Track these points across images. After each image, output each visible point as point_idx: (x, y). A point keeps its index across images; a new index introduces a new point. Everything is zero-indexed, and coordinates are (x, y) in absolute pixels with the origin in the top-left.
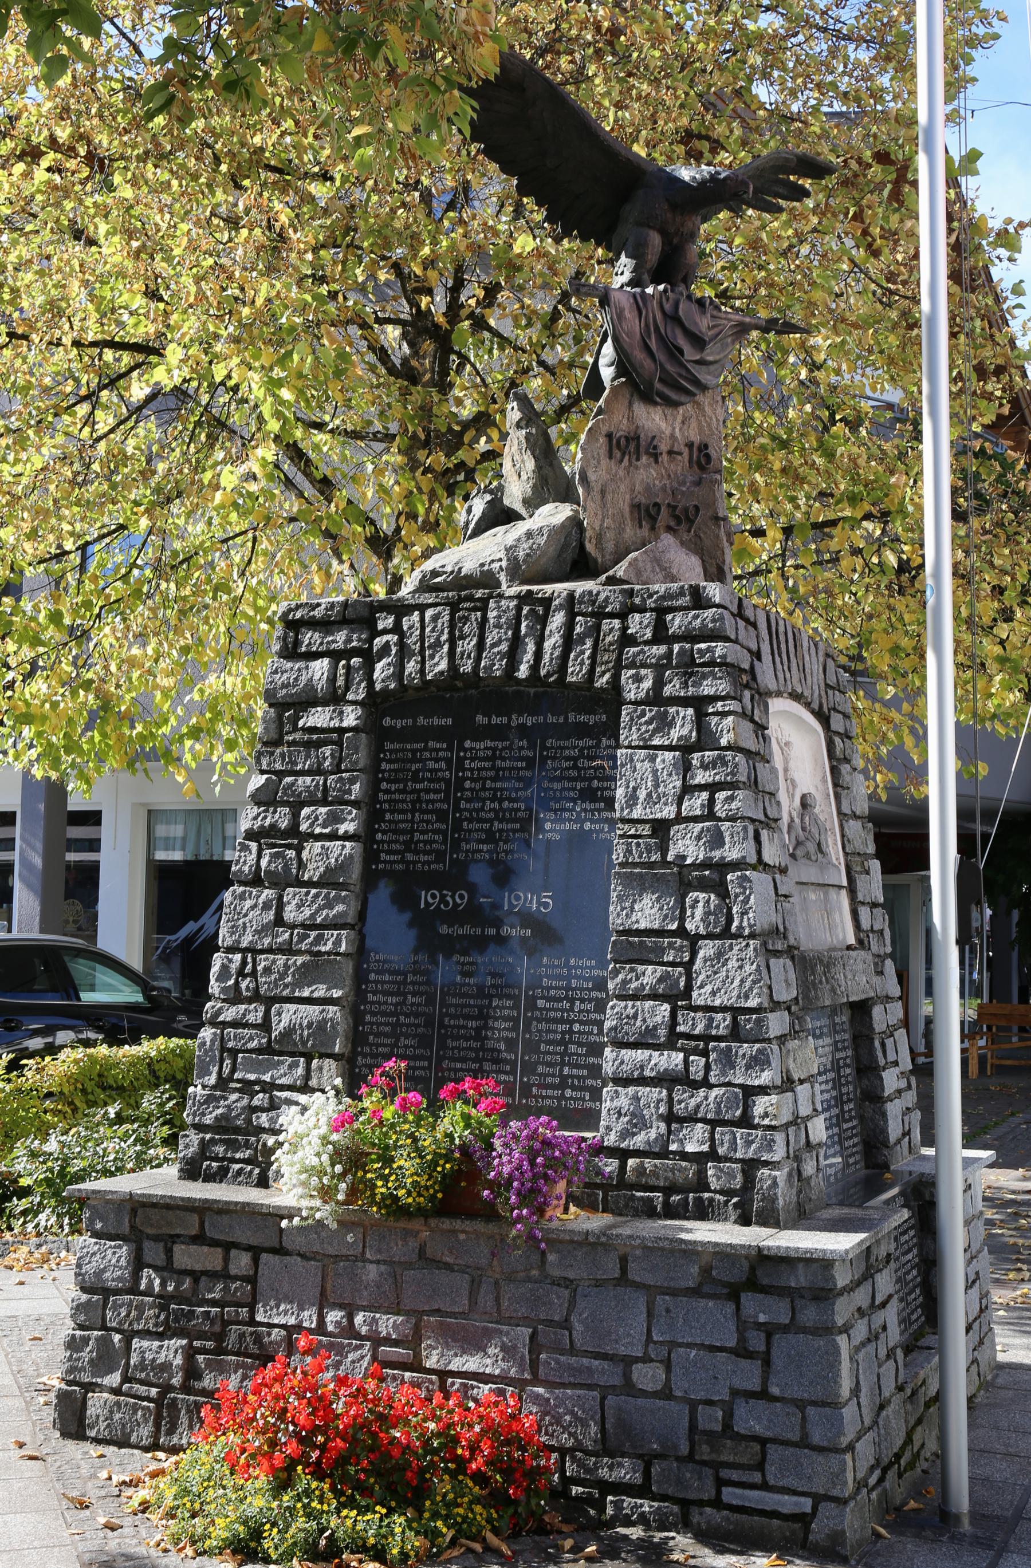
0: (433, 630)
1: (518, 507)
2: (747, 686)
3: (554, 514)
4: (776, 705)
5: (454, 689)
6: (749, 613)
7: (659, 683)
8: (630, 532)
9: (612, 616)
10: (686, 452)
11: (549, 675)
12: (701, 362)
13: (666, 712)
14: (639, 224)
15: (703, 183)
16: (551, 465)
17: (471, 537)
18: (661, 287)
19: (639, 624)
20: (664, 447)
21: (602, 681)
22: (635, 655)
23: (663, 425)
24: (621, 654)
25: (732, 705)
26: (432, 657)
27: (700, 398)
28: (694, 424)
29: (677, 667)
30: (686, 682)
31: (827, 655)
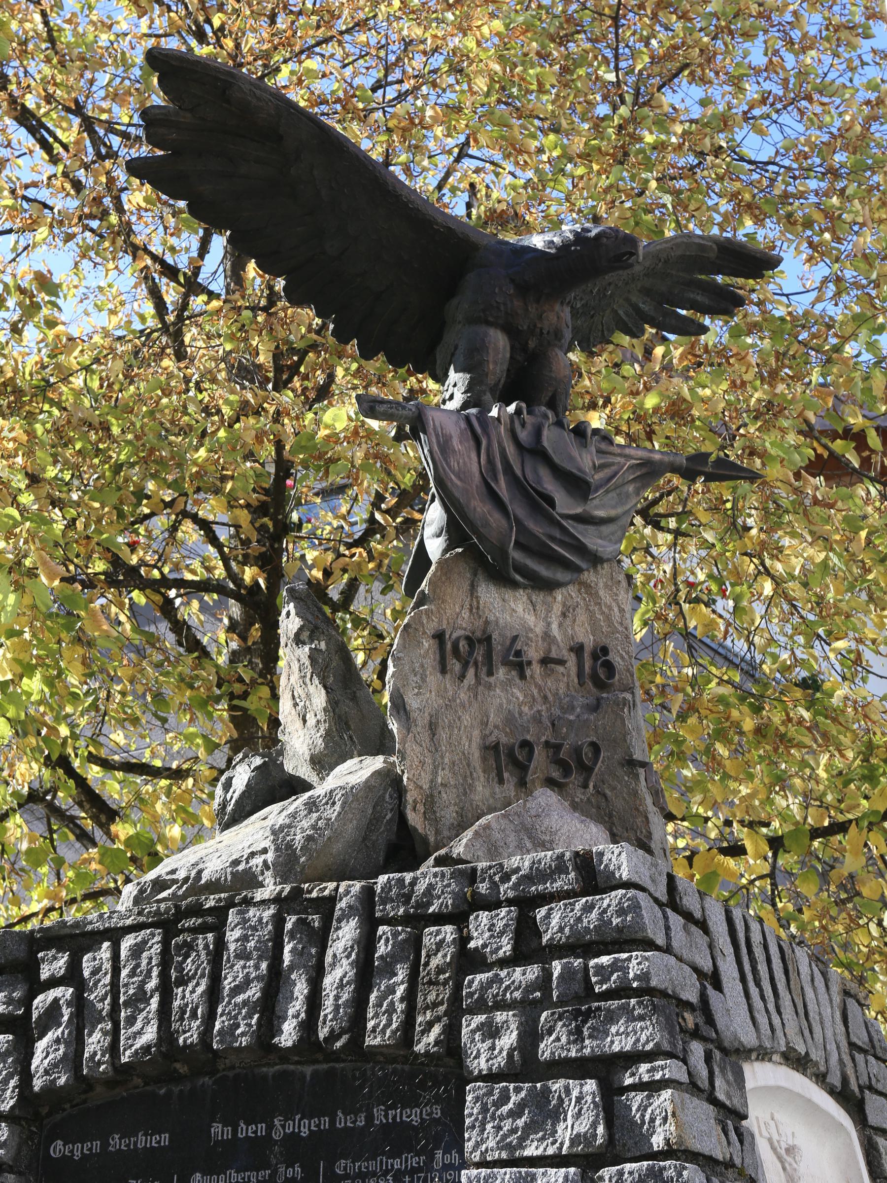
0: (132, 974)
1: (305, 772)
2: (696, 1034)
3: (356, 771)
4: (759, 1075)
5: (175, 1078)
6: (691, 902)
7: (530, 1036)
8: (482, 790)
9: (440, 919)
10: (572, 661)
11: (333, 1036)
12: (584, 519)
13: (547, 1091)
14: (472, 321)
15: (565, 247)
16: (354, 698)
17: (226, 826)
18: (511, 408)
19: (488, 930)
20: (533, 653)
21: (427, 1041)
22: (485, 987)
23: (531, 619)
24: (458, 987)
25: (670, 1069)
26: (131, 1020)
27: (589, 576)
28: (582, 617)
29: (561, 1003)
30: (579, 1031)
31: (846, 993)
